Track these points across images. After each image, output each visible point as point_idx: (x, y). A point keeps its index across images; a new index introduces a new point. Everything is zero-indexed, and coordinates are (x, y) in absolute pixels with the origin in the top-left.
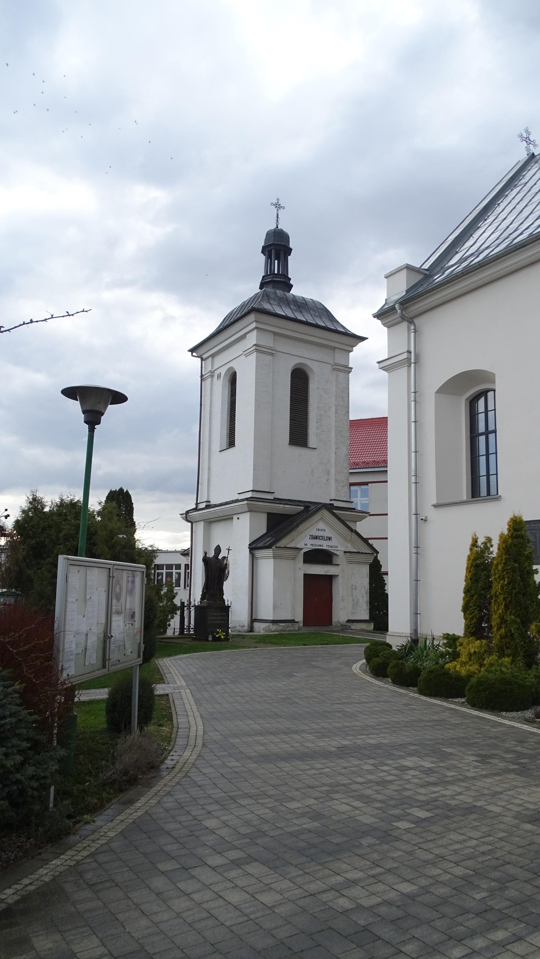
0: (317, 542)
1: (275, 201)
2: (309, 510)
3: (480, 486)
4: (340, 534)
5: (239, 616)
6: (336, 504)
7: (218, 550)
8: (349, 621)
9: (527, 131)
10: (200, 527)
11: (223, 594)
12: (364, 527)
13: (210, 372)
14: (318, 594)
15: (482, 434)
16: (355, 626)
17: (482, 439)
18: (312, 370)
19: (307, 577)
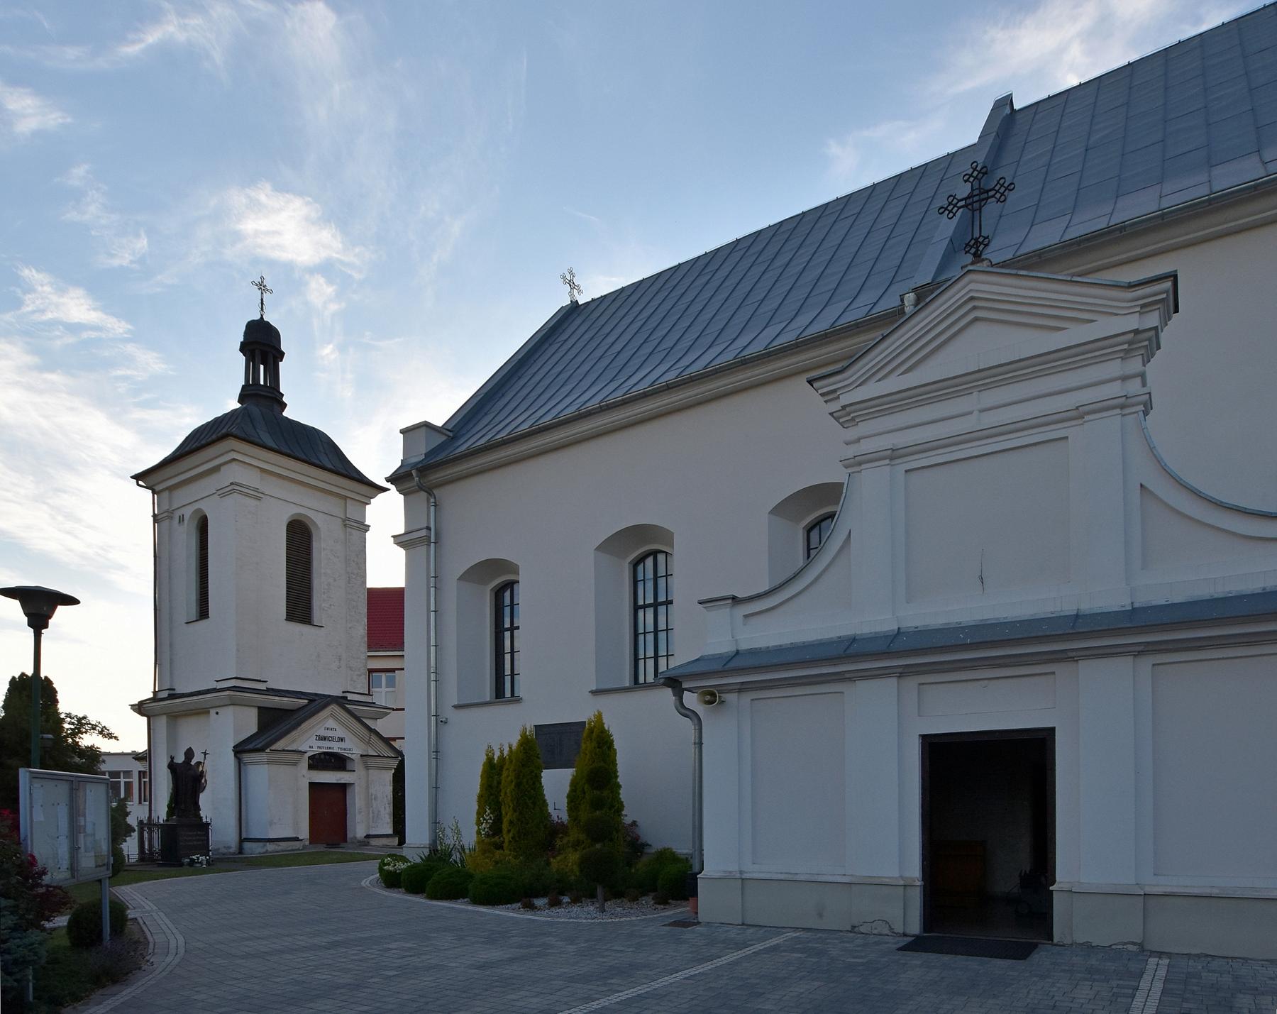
0: (327, 744)
1: (258, 280)
2: (316, 703)
3: (503, 689)
4: (355, 734)
5: (223, 832)
6: (350, 697)
7: (189, 754)
8: (368, 836)
9: (571, 272)
10: (162, 722)
11: (199, 810)
12: (385, 726)
13: (167, 511)
14: (329, 807)
15: (507, 629)
16: (374, 842)
17: (507, 634)
18: (315, 523)
19: (313, 786)
